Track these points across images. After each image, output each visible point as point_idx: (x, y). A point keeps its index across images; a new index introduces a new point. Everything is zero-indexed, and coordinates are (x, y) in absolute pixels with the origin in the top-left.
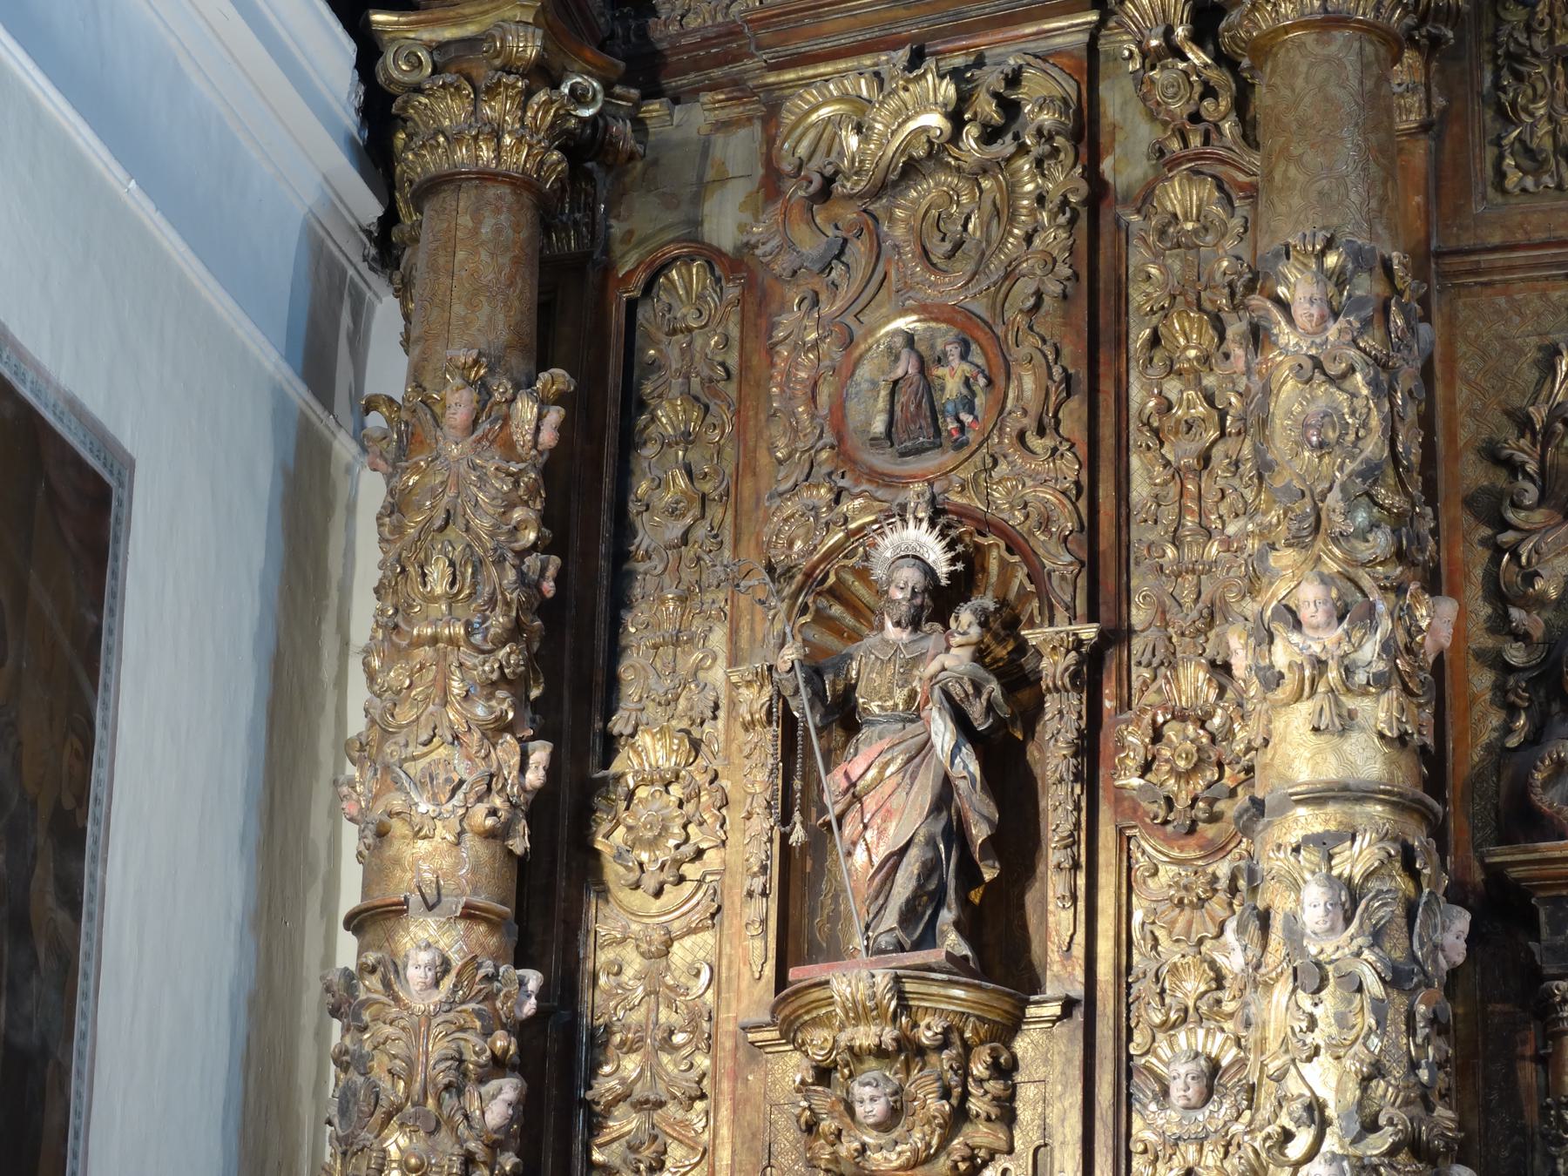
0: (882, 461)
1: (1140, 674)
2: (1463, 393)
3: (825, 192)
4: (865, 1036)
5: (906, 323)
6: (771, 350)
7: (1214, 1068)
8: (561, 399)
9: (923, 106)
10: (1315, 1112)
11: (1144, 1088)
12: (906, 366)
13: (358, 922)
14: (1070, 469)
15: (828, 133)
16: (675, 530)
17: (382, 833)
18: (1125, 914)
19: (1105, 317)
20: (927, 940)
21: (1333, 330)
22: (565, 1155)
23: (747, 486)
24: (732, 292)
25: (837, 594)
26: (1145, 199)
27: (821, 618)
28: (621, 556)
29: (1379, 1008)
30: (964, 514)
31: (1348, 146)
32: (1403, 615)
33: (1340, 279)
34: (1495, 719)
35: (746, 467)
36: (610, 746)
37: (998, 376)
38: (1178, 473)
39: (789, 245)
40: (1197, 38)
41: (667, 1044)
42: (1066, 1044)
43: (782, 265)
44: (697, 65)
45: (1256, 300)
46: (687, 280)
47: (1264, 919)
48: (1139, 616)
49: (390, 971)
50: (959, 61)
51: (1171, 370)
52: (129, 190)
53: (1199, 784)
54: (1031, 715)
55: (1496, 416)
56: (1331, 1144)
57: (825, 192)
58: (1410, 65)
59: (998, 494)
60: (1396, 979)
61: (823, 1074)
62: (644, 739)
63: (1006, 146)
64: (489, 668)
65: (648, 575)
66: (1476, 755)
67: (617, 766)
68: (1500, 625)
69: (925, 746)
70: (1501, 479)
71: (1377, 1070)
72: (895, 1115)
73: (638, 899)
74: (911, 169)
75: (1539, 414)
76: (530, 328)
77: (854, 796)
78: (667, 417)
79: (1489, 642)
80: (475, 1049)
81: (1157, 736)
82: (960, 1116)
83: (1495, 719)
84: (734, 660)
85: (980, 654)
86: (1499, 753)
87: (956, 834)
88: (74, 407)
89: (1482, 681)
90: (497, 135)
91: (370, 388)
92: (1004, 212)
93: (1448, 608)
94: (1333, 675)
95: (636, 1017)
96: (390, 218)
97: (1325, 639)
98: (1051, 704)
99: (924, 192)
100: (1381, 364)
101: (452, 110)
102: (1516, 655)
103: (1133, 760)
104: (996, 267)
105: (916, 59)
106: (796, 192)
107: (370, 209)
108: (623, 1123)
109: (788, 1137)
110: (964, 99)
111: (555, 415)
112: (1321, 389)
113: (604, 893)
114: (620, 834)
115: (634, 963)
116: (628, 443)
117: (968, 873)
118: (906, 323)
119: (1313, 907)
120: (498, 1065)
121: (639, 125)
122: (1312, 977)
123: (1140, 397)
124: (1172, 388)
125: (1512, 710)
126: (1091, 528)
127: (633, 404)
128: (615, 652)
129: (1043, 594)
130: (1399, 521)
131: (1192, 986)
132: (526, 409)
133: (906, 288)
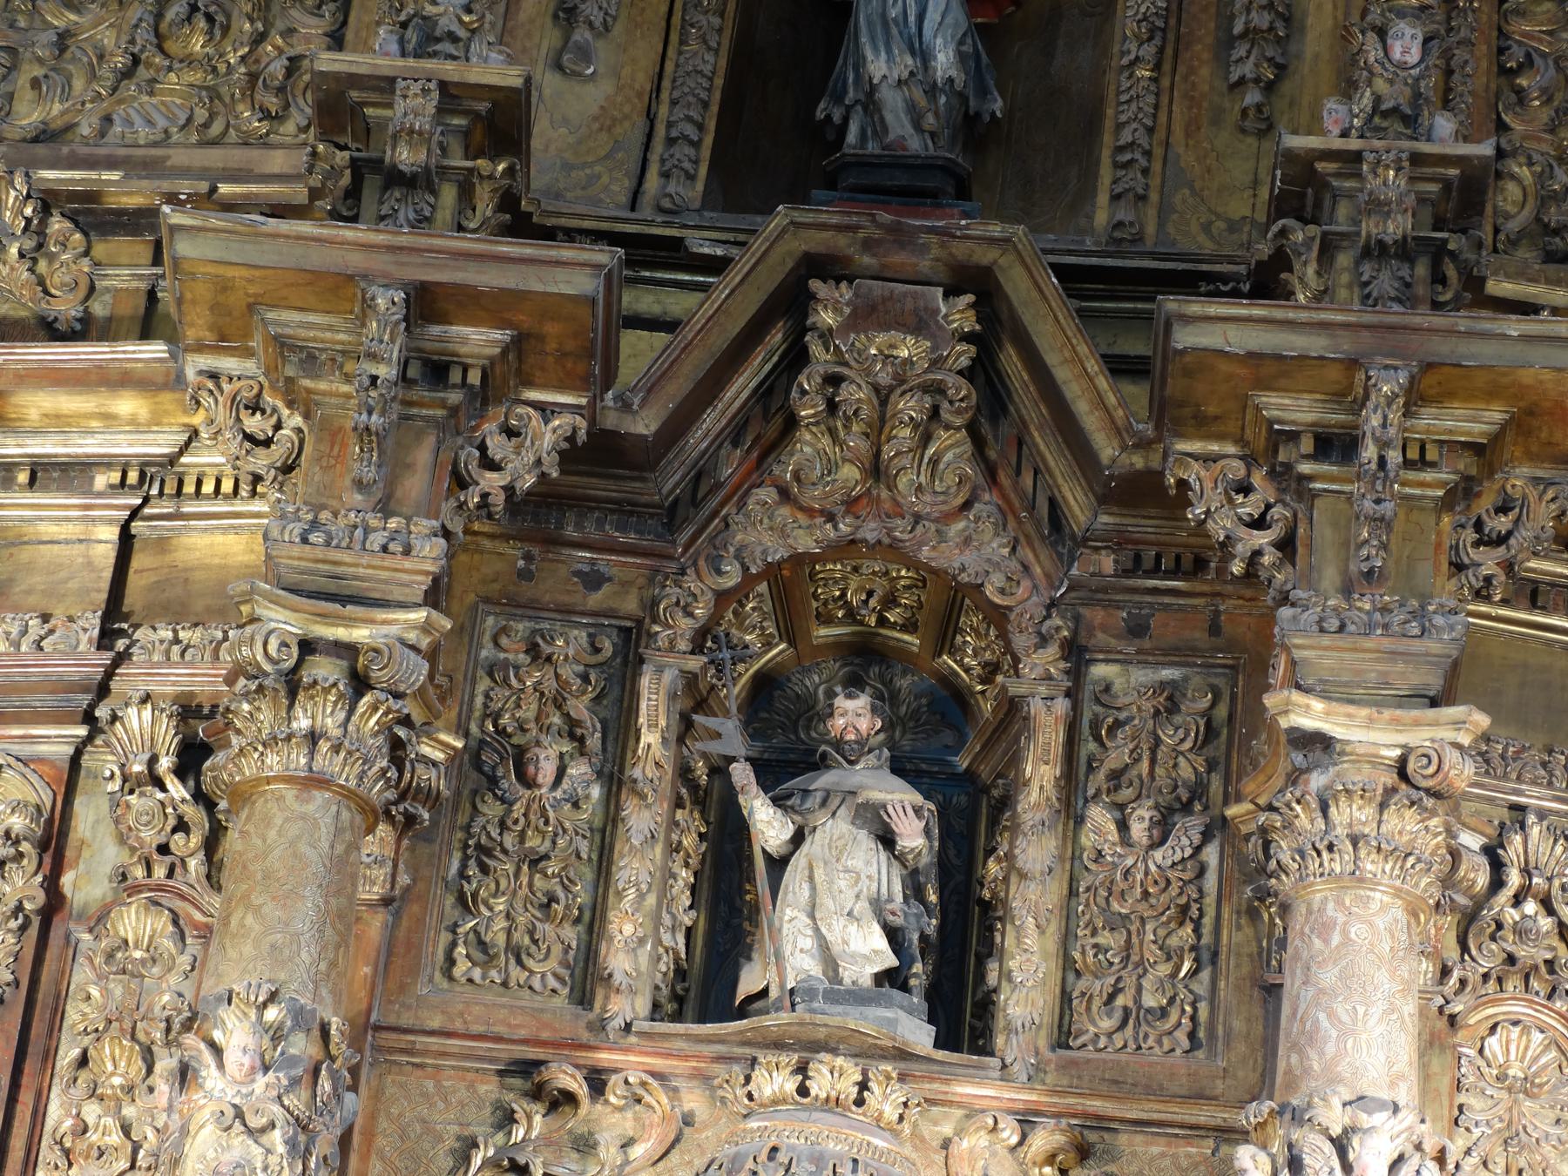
18: (50, 519)
19: (38, 1028)
21: (261, 1081)
26: (99, 920)
33: (277, 1035)
40: (180, 772)
45: (190, 1039)
100: (302, 1125)
124: (91, 1111)
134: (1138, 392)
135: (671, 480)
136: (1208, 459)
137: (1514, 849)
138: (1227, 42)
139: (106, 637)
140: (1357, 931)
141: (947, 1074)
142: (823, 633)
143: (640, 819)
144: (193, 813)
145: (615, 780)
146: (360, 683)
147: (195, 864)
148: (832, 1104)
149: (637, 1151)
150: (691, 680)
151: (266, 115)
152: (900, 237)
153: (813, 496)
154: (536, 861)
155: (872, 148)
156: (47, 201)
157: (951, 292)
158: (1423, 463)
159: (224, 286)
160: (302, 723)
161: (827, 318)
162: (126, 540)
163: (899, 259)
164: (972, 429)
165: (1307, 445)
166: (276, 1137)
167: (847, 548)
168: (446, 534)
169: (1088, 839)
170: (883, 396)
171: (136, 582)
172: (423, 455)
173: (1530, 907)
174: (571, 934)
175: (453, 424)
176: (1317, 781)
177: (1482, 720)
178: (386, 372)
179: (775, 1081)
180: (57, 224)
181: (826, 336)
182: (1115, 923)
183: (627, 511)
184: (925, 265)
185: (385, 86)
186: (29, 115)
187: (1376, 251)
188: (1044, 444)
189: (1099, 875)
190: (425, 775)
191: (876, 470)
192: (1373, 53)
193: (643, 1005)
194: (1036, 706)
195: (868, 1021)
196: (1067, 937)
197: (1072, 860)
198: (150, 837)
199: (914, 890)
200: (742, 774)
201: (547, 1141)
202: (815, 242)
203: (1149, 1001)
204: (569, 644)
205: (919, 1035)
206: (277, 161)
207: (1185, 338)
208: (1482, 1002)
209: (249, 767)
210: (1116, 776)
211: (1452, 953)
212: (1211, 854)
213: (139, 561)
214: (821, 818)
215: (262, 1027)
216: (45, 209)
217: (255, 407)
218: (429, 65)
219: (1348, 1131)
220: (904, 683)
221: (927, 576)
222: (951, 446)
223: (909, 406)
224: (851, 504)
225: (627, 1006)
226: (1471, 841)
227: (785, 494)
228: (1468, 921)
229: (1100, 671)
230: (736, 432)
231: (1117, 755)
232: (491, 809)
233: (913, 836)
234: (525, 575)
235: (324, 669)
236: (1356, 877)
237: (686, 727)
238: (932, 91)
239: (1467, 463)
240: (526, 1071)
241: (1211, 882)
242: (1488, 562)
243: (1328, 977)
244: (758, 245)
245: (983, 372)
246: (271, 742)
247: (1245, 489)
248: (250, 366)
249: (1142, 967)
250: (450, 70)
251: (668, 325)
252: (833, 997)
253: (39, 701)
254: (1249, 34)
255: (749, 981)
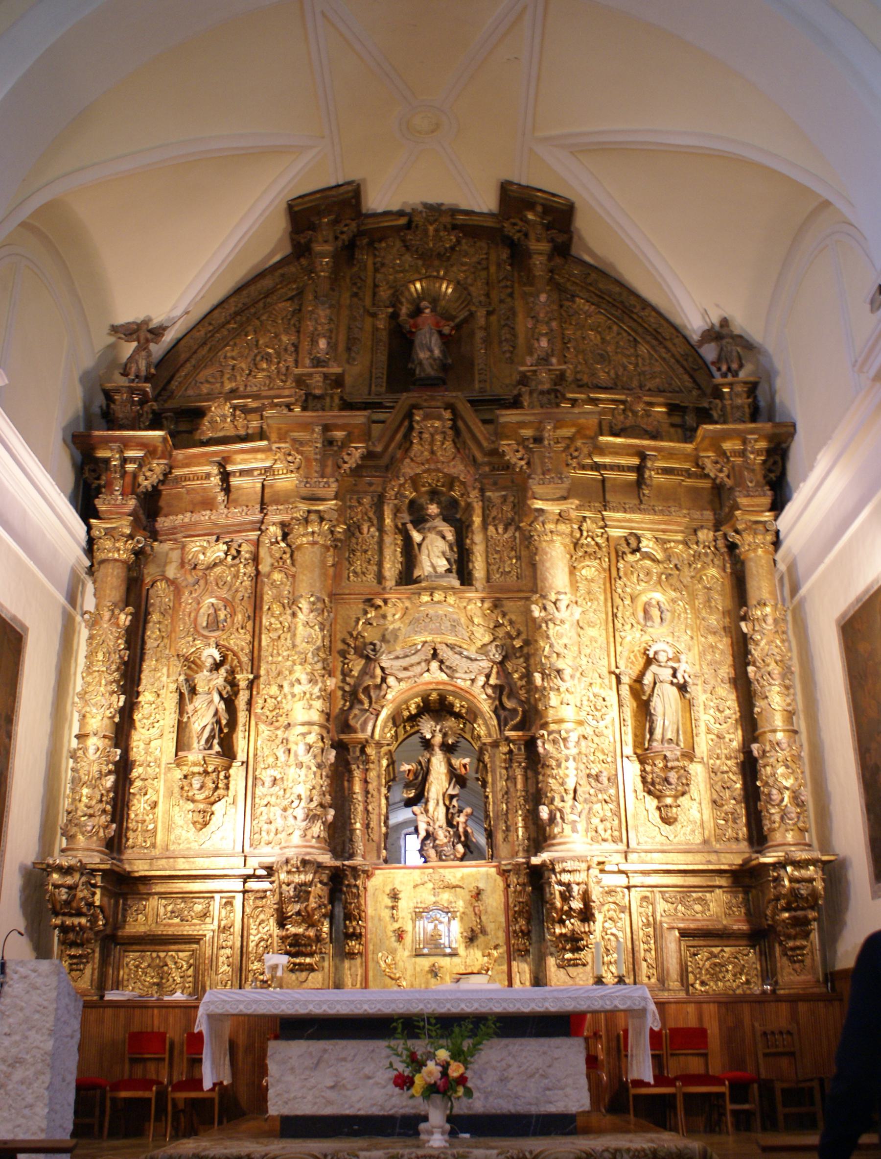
0: (206, 633)
1: (262, 686)
2: (338, 627)
3: (195, 568)
4: (196, 769)
5: (213, 600)
6: (180, 604)
7: (275, 779)
8: (131, 614)
9: (219, 551)
10: (299, 797)
11: (259, 783)
12: (211, 611)
13: (78, 737)
14: (248, 637)
15: (196, 555)
16: (156, 644)
17: (84, 716)
18: (256, 741)
19: (258, 602)
20: (210, 748)
21: (312, 615)
22: (124, 790)
23: (173, 635)
24: (172, 588)
25: (193, 662)
26: (268, 576)
27: (189, 668)
28: (143, 648)
29: (315, 773)
30: (224, 646)
31: (317, 572)
32: (324, 682)
33: (313, 603)
34: (342, 702)
35: (173, 630)
36: (138, 694)
37: (233, 614)
38: (273, 640)
39: (186, 579)
41: (149, 766)
42: (242, 771)
43: (184, 584)
44: (166, 534)
45: (294, 607)
46: (161, 585)
47: (289, 751)
48: (262, 672)
49: (85, 750)
50: (227, 540)
51: (273, 616)
52: (31, 564)
53: (274, 713)
54: (236, 694)
55: (345, 633)
56: (303, 804)
57: (195, 568)
58: (331, 551)
59: (232, 642)
60: (319, 766)
61: (186, 777)
62: (146, 693)
63: (237, 561)
64: (111, 678)
65: (149, 653)
66: (337, 710)
67: (140, 699)
68: (344, 681)
69: (212, 701)
70: (346, 647)
71: (314, 788)
72: (201, 787)
73: (143, 731)
74: (215, 565)
75: (355, 633)
76: (124, 597)
77: (195, 711)
78: (155, 617)
79: (341, 684)
80: (105, 769)
81: (265, 701)
82: (217, 788)
83: (342, 702)
84: (168, 677)
85: (225, 681)
86: (342, 709)
87: (218, 722)
88: (14, 618)
89: (340, 693)
90: (119, 550)
91: (85, 609)
92: (236, 576)
93: (334, 680)
94: (308, 696)
95: (142, 758)
96: (92, 566)
97: (306, 687)
98: (241, 692)
99: (218, 570)
100: (321, 624)
101: (108, 544)
102: (347, 688)
103: (260, 706)
104: (234, 589)
105: (217, 540)
106: (188, 567)
107: (88, 564)
108: (138, 783)
109: (177, 790)
110: (229, 550)
111: (129, 618)
112: (308, 629)
113: (135, 729)
114: (140, 716)
115: (142, 746)
116: (146, 622)
117: (221, 731)
118: (213, 600)
119: (301, 749)
120: (110, 772)
121: (152, 548)
122: (300, 765)
123: (265, 622)
124: (273, 620)
125: (346, 701)
126: (252, 652)
127: (147, 613)
128: (140, 672)
129: (241, 666)
130: (324, 660)
131: (271, 760)
132: (122, 617)
133: (212, 592)
134: (491, 427)
135: (385, 461)
136: (509, 445)
137: (585, 527)
138: (500, 342)
139: (261, 512)
140: (554, 553)
141: (464, 592)
142: (424, 489)
143: (388, 540)
144: (288, 550)
145: (381, 529)
146: (322, 519)
147: (289, 561)
148: (439, 602)
149: (397, 617)
150: (395, 505)
151: (283, 381)
152: (432, 398)
153: (419, 460)
154: (366, 551)
155: (423, 375)
156: (235, 408)
157: (445, 409)
158: (558, 442)
159: (279, 429)
160: (310, 530)
161: (418, 418)
162: (263, 486)
163: (433, 404)
164: (454, 441)
165: (531, 441)
166: (317, 627)
167: (427, 471)
168: (337, 481)
169: (489, 533)
170: (432, 435)
171: (266, 496)
172: (330, 463)
173: (589, 539)
174: (375, 568)
175: (337, 454)
176: (541, 519)
177: (577, 502)
178: (319, 445)
179: (425, 598)
180: (238, 413)
181: (418, 422)
182: (497, 552)
183: (376, 468)
184: (439, 404)
185: (310, 375)
186: (228, 386)
187: (542, 393)
188: (470, 443)
189: (492, 542)
190: (339, 536)
191: (433, 452)
192: (536, 345)
193: (394, 583)
194: (475, 505)
195: (444, 582)
196: (487, 557)
197: (487, 539)
198: (277, 555)
199: (451, 549)
200: (410, 526)
201: (376, 617)
202: (412, 401)
203: (507, 569)
204: (366, 500)
205: (456, 583)
206: (286, 392)
207: (502, 420)
208: (580, 562)
209: (299, 542)
210: (494, 518)
211: (573, 551)
212: (517, 534)
213: (267, 491)
214: (429, 535)
215: (310, 602)
216: (235, 410)
217: (289, 455)
218: (320, 369)
219: (557, 600)
220: (443, 499)
221: (446, 475)
222: (448, 444)
223: (438, 437)
224: (428, 461)
225: (390, 583)
226: (576, 526)
227: (412, 460)
228: (576, 545)
229: (488, 494)
230: (400, 447)
231: (494, 513)
232: (354, 540)
233: (450, 537)
234: (355, 485)
235: (313, 517)
236: (552, 541)
237: (395, 515)
238: (435, 360)
239: (567, 441)
240: (369, 602)
241: (518, 541)
242: (574, 463)
243: (548, 565)
244: (400, 402)
245: (455, 428)
246: (303, 535)
247: (518, 451)
248: (287, 445)
249: (504, 562)
250: (325, 370)
251: (383, 422)
252: (436, 577)
253: (249, 527)
254: (506, 340)
255: (417, 573)
